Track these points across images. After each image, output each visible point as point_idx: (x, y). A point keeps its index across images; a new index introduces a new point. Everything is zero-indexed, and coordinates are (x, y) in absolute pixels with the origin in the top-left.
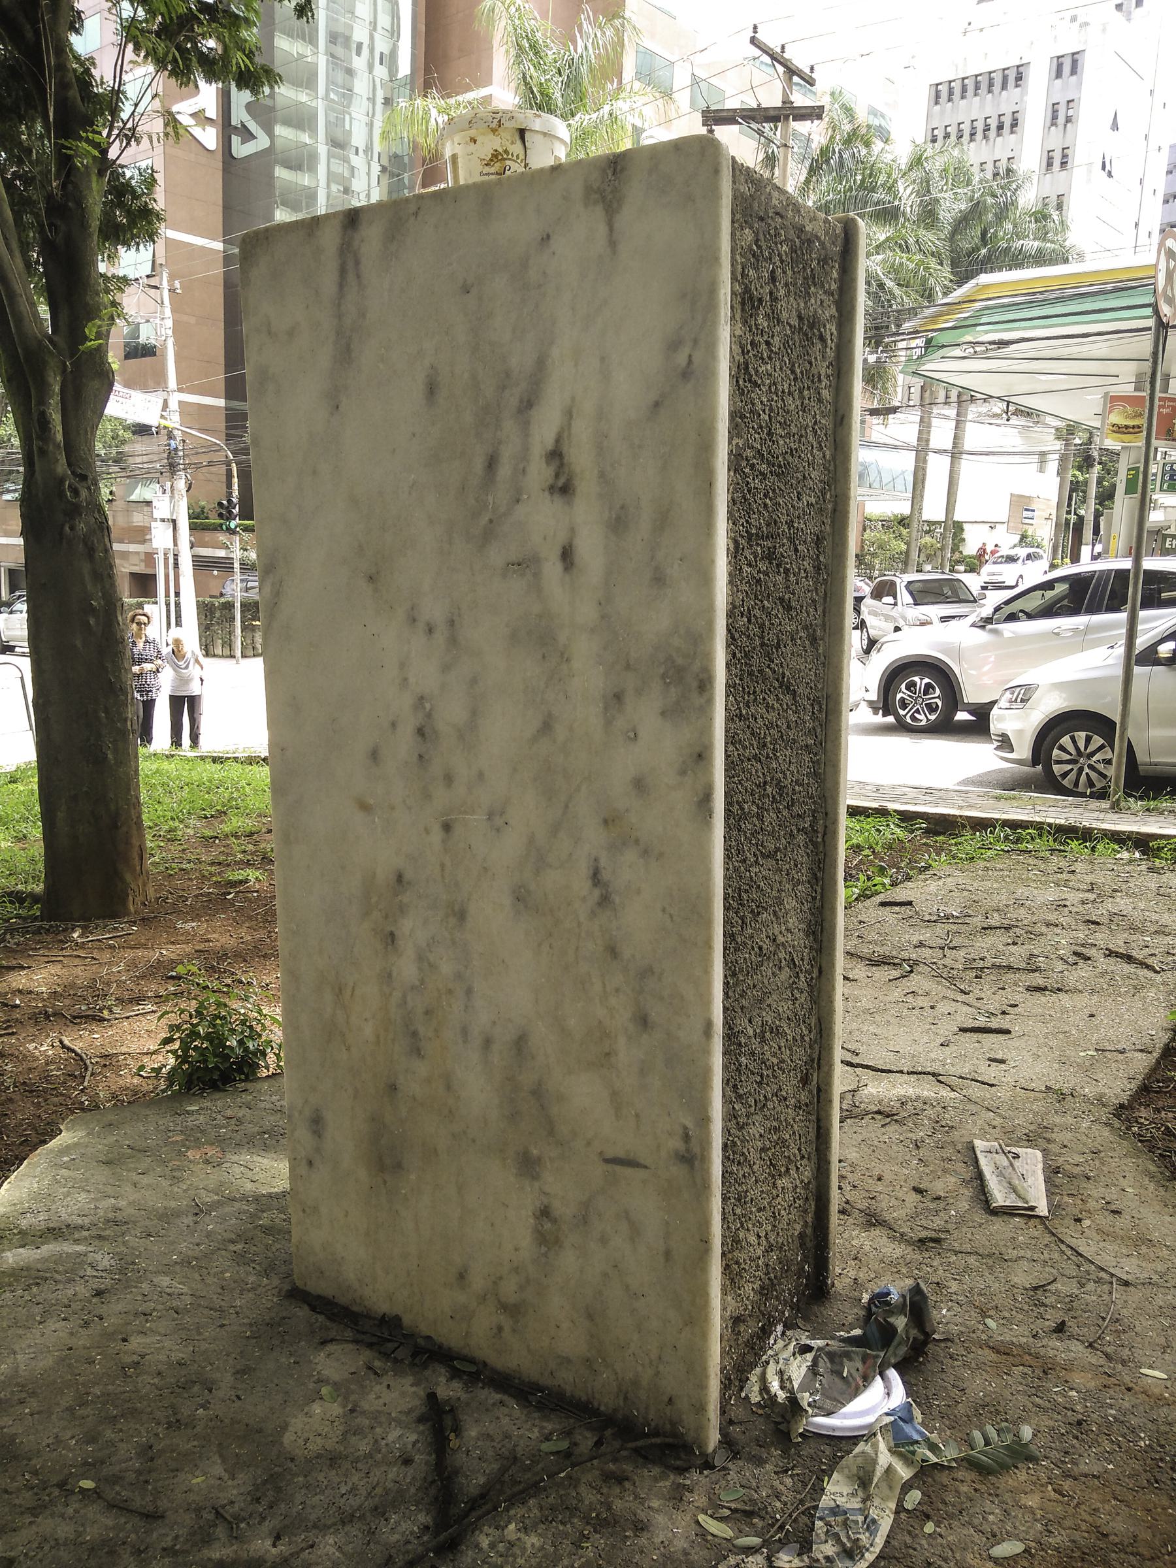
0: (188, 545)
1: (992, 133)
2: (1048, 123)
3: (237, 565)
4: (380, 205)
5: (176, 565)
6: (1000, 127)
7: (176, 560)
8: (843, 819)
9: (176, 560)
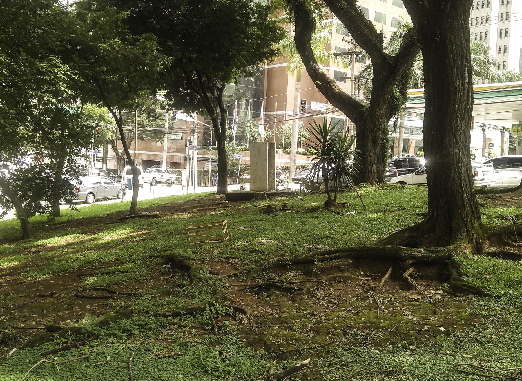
0: (510, 50)
1: (480, 7)
2: (501, 4)
3: (210, 159)
4: (59, 211)
5: (193, 160)
6: (483, 5)
7: (193, 158)
8: (503, 156)
9: (193, 158)
